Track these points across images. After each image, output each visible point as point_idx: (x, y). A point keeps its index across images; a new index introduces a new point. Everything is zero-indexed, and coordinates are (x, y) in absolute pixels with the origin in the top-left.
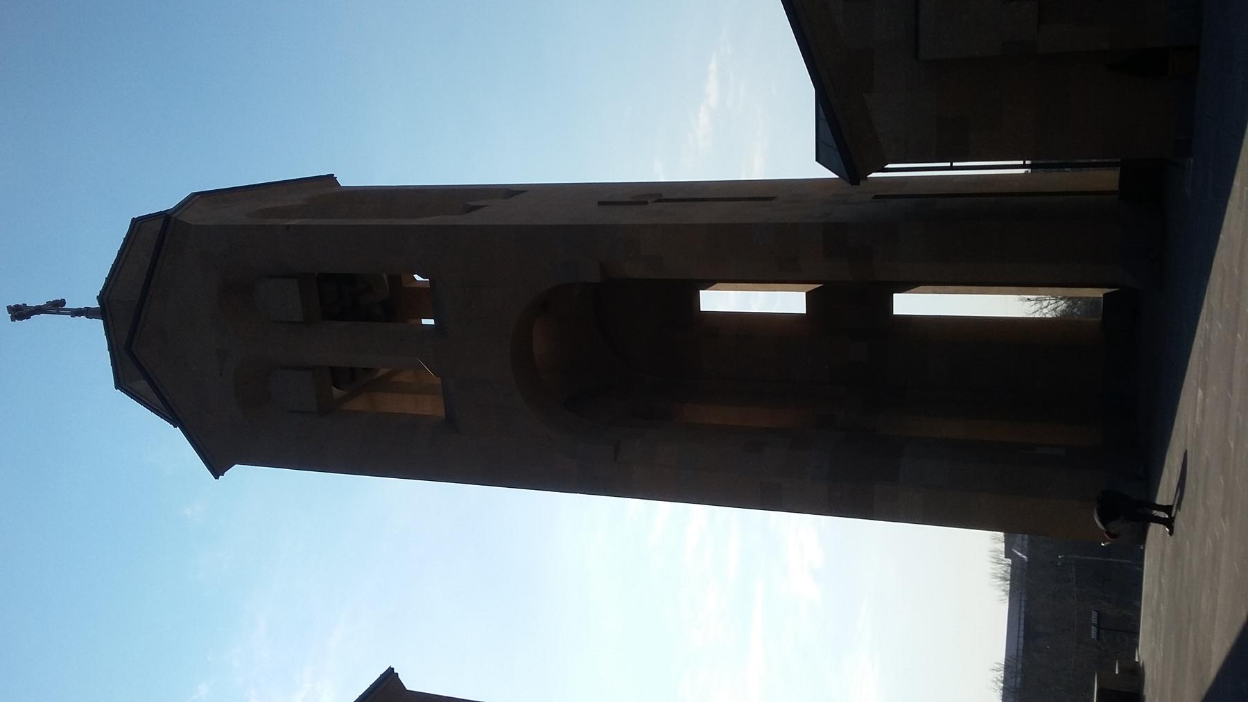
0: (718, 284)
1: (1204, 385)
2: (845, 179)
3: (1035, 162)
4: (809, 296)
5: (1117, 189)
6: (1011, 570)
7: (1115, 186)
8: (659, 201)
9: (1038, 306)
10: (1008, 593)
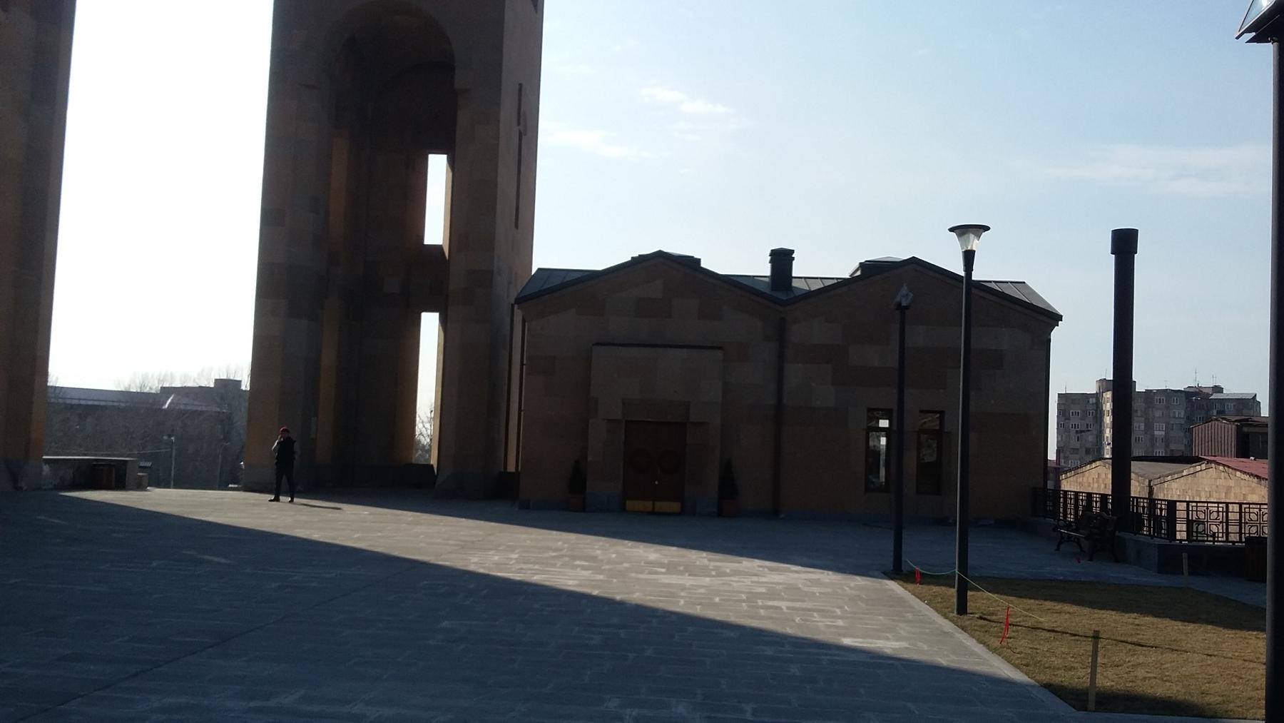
1: (371, 514)
4: (439, 248)
6: (152, 393)
8: (520, 134)
9: (425, 420)
10: (128, 390)
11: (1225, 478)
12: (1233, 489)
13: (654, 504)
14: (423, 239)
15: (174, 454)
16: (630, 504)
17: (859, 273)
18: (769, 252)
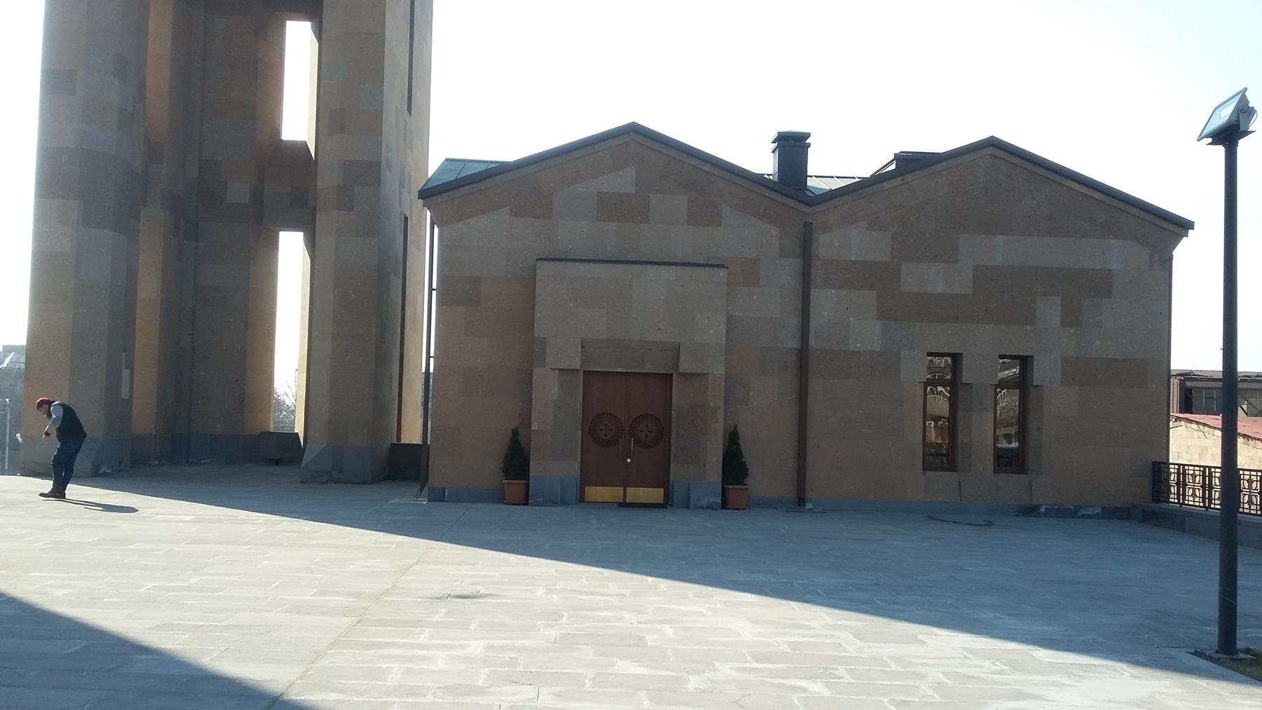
0: (317, 44)
2: (423, 187)
3: (431, 376)
5: (1221, 377)
7: (1221, 386)
11: (1199, 437)
12: (1209, 450)
13: (625, 491)
14: (278, 132)
15: (9, 418)
16: (597, 493)
17: (893, 167)
18: (774, 135)
